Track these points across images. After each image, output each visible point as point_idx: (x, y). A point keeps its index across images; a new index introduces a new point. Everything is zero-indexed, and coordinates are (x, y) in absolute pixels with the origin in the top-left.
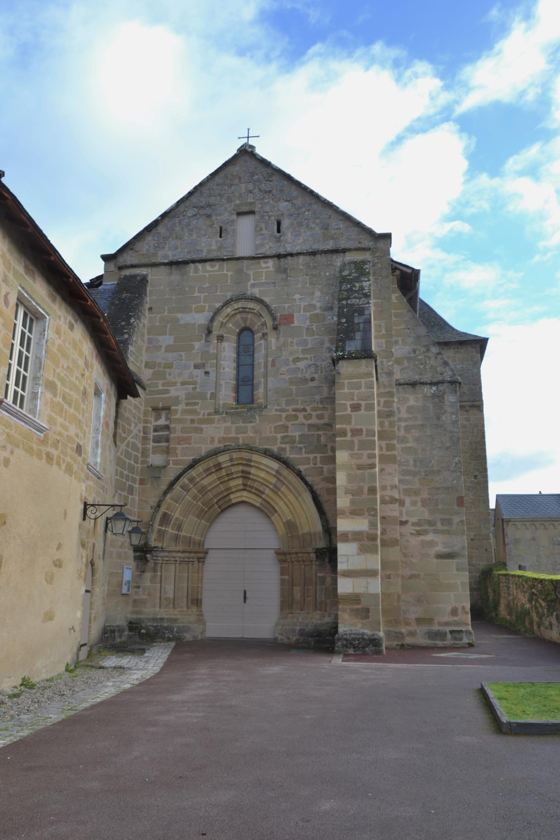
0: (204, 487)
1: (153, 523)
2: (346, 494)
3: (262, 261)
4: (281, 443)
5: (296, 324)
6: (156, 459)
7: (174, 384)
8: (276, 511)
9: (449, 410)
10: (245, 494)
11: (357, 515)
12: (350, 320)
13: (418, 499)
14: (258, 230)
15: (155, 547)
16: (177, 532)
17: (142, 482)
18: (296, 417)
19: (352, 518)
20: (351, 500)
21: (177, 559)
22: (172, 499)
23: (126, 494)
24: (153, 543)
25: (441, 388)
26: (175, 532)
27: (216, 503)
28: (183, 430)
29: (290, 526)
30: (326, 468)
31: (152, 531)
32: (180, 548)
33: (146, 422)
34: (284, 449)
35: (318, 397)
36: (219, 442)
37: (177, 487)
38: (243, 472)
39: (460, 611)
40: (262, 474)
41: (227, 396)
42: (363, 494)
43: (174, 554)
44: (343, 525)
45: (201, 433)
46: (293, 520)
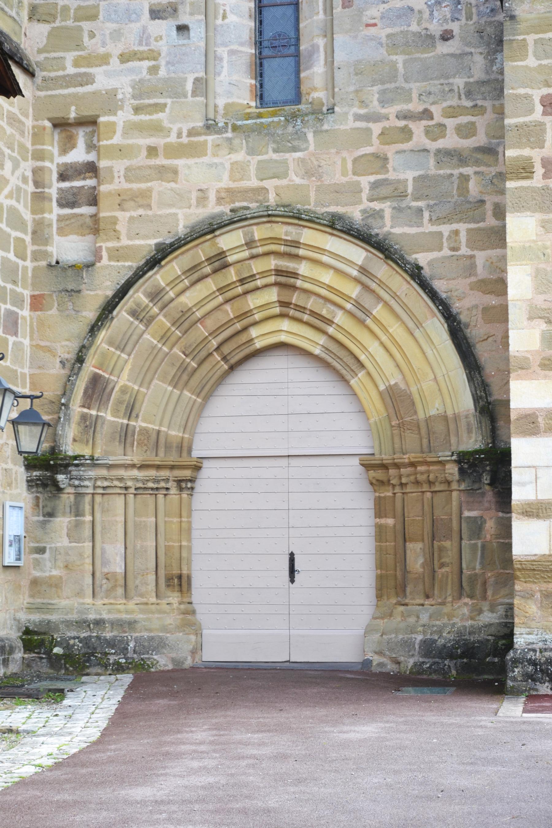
0: (186, 312)
1: (69, 400)
2: (531, 318)
4: (371, 200)
6: (70, 248)
7: (104, 60)
8: (362, 366)
10: (285, 324)
15: (76, 458)
16: (125, 421)
17: (37, 303)
18: (407, 133)
24: (70, 448)
26: (121, 421)
27: (217, 349)
28: (131, 174)
29: (397, 400)
31: (68, 418)
32: (135, 456)
33: (39, 156)
34: (378, 215)
36: (220, 200)
37: (122, 314)
38: (279, 272)
40: (327, 277)
41: (234, 85)
43: (122, 472)
46: (403, 386)
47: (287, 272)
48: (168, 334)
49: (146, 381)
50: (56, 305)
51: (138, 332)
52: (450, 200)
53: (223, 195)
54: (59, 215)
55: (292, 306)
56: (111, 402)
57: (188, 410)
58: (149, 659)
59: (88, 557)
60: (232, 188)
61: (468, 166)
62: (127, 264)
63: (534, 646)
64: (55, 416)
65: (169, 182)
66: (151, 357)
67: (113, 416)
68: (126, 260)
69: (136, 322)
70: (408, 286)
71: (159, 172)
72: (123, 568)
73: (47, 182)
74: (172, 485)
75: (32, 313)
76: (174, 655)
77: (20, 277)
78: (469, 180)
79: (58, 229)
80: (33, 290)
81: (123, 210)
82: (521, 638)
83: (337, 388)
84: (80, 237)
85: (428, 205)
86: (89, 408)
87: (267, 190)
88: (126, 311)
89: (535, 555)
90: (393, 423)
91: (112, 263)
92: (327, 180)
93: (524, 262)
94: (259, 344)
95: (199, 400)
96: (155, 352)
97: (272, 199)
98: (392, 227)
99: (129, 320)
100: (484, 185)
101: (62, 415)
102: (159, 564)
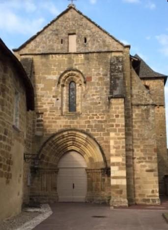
0: (57, 144)
3: (79, 55)
5: (93, 81)
7: (45, 104)
9: (151, 115)
10: (73, 147)
12: (115, 82)
13: (139, 149)
14: (77, 41)
17: (33, 142)
18: (93, 118)
25: (149, 107)
28: (49, 122)
29: (91, 159)
30: (105, 137)
32: (48, 167)
33: (34, 118)
34: (89, 130)
35: (101, 110)
38: (72, 138)
39: (155, 191)
40: (80, 139)
41: (65, 108)
44: (113, 160)
83: (82, 157)
92: (81, 124)
97: (72, 127)
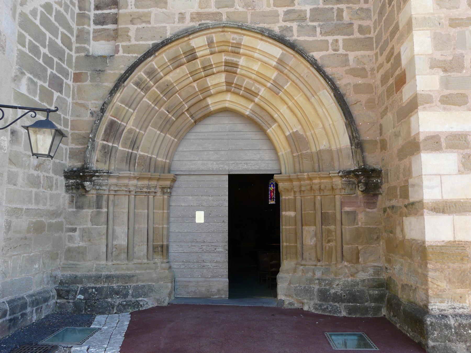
0: (169, 85)
1: (94, 136)
2: (432, 67)
4: (285, 21)
6: (99, 48)
8: (275, 121)
10: (229, 97)
11: (454, 104)
15: (97, 171)
16: (130, 151)
17: (77, 78)
19: (444, 109)
20: (441, 78)
21: (132, 188)
22: (122, 101)
23: (46, 85)
24: (94, 166)
26: (127, 150)
27: (187, 110)
31: (93, 148)
34: (290, 29)
36: (192, 19)
37: (130, 84)
38: (227, 63)
42: (463, 68)
43: (126, 181)
45: (165, 8)
46: (301, 132)
47: (232, 63)
48: (159, 99)
49: (144, 127)
50: (89, 79)
51: (140, 96)
52: (332, 22)
53: (195, 16)
54: (94, 29)
55: (233, 85)
56: (122, 139)
57: (169, 145)
58: (141, 301)
59: (104, 234)
60: (200, 13)
61: (342, 3)
62: (134, 55)
63: (446, 312)
64: (86, 146)
65: (162, 8)
66: (148, 112)
67: (123, 147)
68: (134, 53)
69: (139, 90)
70: (308, 71)
71: (156, 3)
72: (127, 241)
73: (87, 7)
74: (159, 190)
75: (74, 84)
76: (157, 297)
77: (66, 58)
78: (343, 11)
79: (93, 37)
80: (75, 70)
81: (133, 24)
82: (435, 305)
84: (107, 42)
85: (319, 25)
86: (107, 141)
87: (222, 14)
88: (132, 83)
89: (443, 241)
90: (295, 155)
91: (125, 55)
93: (425, 28)
94: (212, 108)
95: (176, 140)
96: (150, 109)
97: (224, 18)
98: (298, 36)
99: (134, 88)
100: (352, 15)
101: (89, 145)
102: (149, 239)
